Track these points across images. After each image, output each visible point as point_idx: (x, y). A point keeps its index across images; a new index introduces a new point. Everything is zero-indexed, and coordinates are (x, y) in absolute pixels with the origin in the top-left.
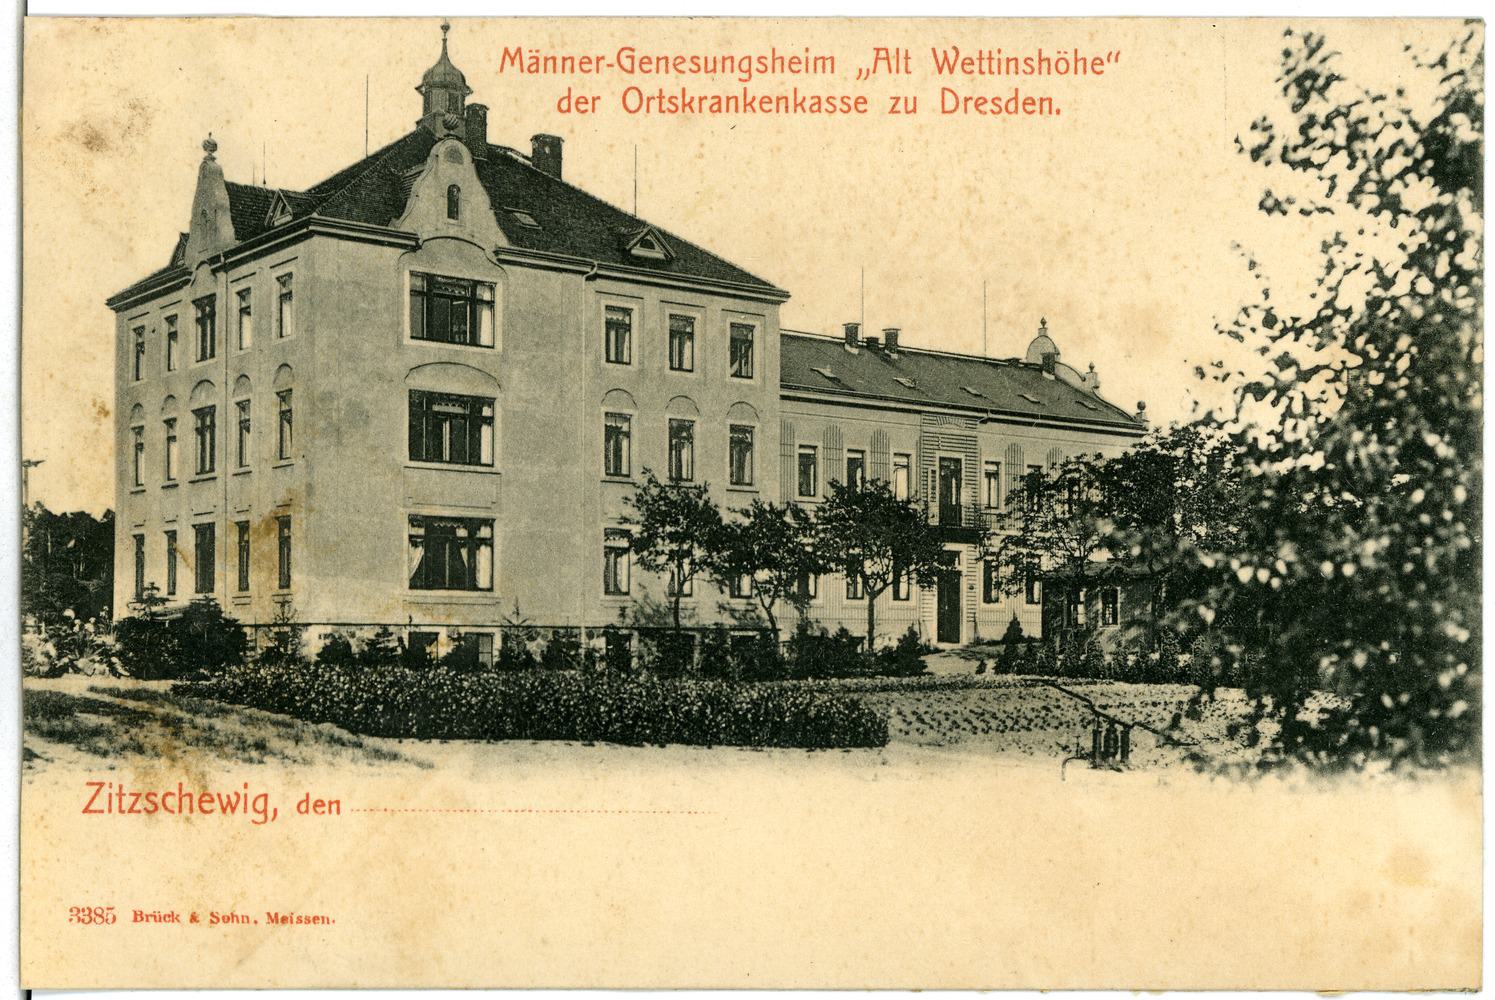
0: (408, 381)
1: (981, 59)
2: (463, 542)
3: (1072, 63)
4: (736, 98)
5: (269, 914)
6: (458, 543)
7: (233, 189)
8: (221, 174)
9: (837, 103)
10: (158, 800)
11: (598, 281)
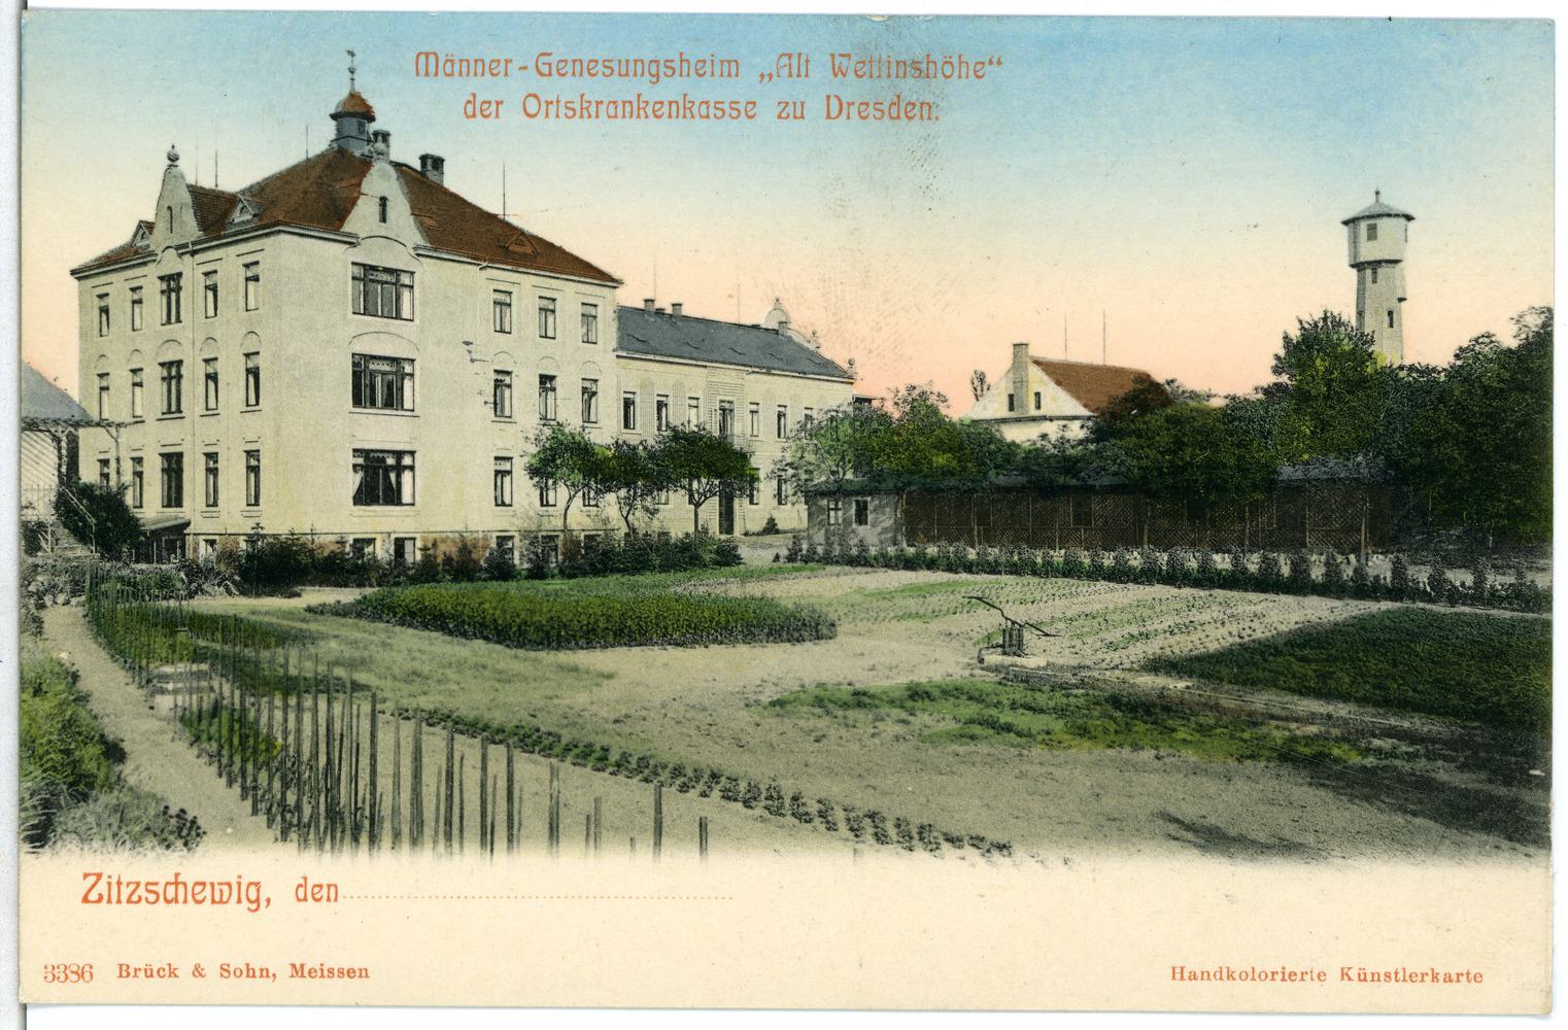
0: (351, 346)
2: (392, 467)
3: (956, 65)
4: (631, 102)
5: (294, 966)
6: (387, 469)
7: (197, 193)
8: (183, 177)
9: (726, 106)
11: (489, 270)
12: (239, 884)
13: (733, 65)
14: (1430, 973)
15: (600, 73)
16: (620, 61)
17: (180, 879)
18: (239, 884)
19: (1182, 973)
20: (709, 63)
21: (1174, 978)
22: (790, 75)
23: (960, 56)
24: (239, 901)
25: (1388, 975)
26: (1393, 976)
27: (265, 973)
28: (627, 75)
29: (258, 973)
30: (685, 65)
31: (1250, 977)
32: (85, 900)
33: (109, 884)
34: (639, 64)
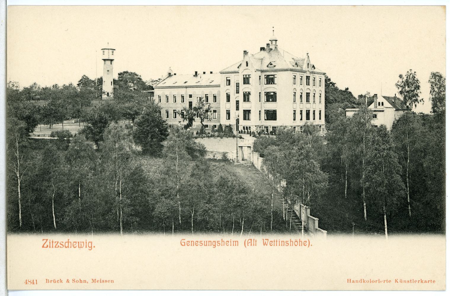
1: (274, 241)
5: (93, 280)
10: (203, 242)
12: (86, 242)
13: (237, 242)
14: (420, 280)
15: (199, 245)
16: (204, 242)
17: (69, 241)
18: (86, 242)
19: (350, 281)
20: (230, 242)
21: (348, 282)
22: (251, 245)
23: (300, 240)
24: (86, 247)
25: (408, 281)
26: (410, 281)
27: (85, 281)
28: (207, 245)
29: (83, 282)
30: (223, 242)
31: (370, 282)
32: (43, 247)
33: (50, 242)
34: (210, 242)
